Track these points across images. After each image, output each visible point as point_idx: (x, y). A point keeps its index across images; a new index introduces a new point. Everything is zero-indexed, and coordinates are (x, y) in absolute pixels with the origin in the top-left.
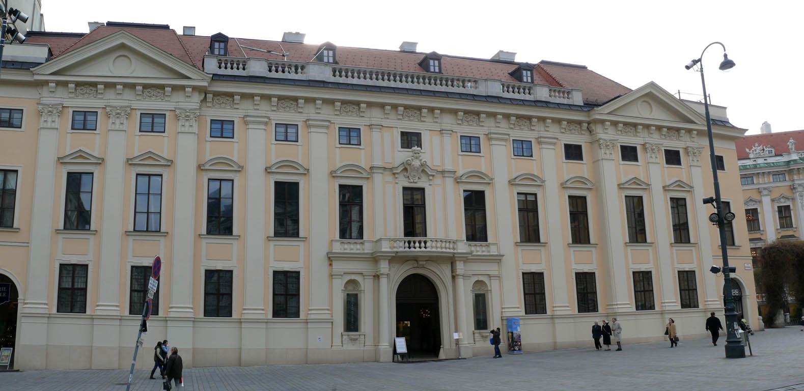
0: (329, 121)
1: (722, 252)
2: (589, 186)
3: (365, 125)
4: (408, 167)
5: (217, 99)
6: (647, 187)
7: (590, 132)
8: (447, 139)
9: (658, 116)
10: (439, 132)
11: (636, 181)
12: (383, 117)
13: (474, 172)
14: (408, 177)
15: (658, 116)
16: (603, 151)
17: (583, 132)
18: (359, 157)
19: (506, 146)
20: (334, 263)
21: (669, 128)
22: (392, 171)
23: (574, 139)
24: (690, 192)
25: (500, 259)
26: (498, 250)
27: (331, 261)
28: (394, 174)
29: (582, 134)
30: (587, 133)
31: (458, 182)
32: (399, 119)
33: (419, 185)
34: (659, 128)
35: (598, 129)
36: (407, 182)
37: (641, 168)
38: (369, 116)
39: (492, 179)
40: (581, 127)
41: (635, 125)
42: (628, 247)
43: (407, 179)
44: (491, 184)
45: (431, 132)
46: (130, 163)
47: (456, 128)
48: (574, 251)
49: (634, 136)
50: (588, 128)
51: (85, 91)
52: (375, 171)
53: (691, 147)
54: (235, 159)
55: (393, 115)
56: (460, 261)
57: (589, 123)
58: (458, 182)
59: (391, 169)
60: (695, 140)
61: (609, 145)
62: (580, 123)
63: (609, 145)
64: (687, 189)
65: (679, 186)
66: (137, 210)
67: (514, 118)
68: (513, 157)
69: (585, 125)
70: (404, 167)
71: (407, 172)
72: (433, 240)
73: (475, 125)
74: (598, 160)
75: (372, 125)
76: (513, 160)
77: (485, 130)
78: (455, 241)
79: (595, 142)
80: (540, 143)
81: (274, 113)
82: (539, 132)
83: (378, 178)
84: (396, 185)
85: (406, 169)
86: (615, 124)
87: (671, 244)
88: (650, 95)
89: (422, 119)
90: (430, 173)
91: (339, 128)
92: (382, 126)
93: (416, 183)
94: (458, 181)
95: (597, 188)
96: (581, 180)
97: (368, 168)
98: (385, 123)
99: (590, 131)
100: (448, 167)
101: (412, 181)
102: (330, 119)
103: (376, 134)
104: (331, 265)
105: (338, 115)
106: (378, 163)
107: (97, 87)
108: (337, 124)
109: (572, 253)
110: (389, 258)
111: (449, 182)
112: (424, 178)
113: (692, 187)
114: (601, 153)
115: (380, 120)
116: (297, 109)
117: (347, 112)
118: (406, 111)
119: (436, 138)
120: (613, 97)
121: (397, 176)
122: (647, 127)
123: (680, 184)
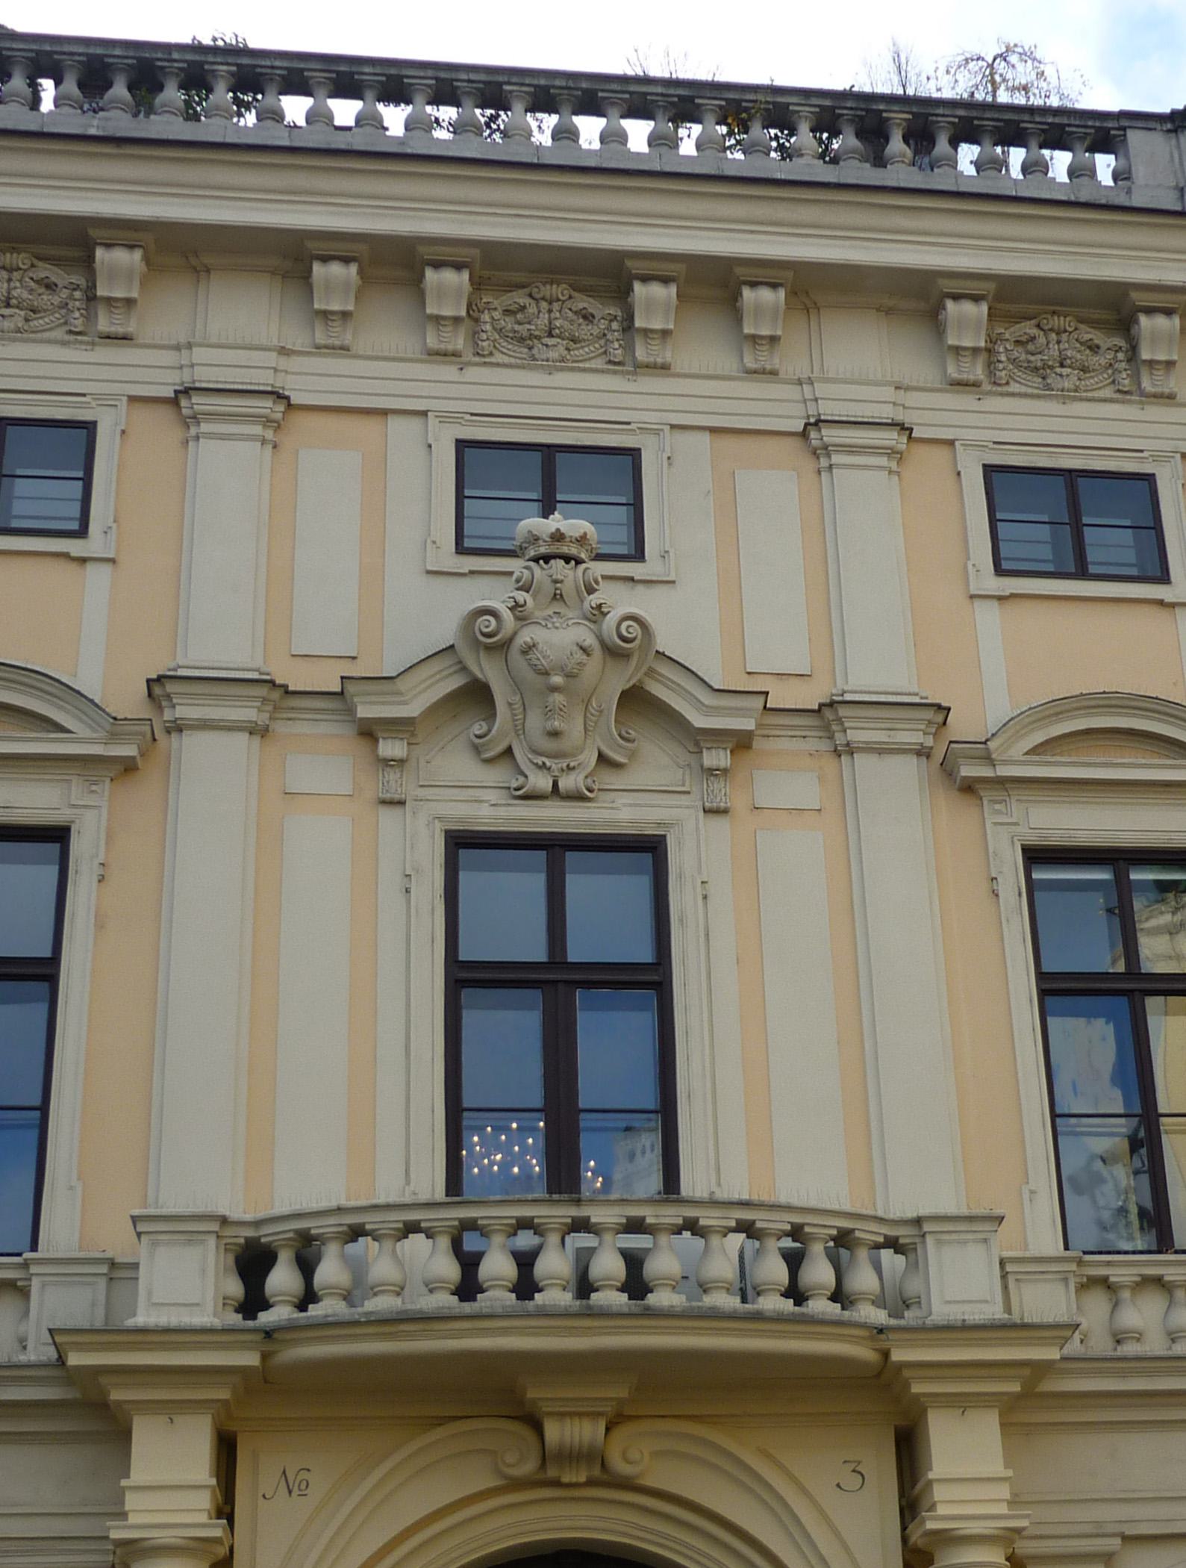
1: (1124, 1096)
4: (490, 671)
5: (507, 312)
8: (865, 493)
10: (166, 413)
12: (298, 339)
13: (1059, 708)
14: (509, 751)
22: (358, 716)
28: (369, 732)
31: (969, 788)
33: (618, 812)
43: (498, 775)
47: (938, 412)
49: (1123, 394)
51: (543, 320)
52: (184, 711)
55: (385, 331)
58: (969, 788)
70: (455, 683)
72: (762, 1219)
73: (1107, 392)
76: (988, 616)
78: (904, 1233)
82: (184, 357)
83: (213, 769)
85: (476, 695)
89: (641, 354)
91: (462, 445)
93: (578, 797)
94: (965, 776)
97: (126, 698)
98: (310, 379)
101: (541, 782)
102: (907, 418)
103: (228, 465)
106: (223, 643)
107: (87, 263)
108: (446, 418)
111: (894, 792)
112: (657, 762)
115: (272, 359)
116: (90, 317)
118: (1010, 333)
119: (774, 487)
121: (390, 748)
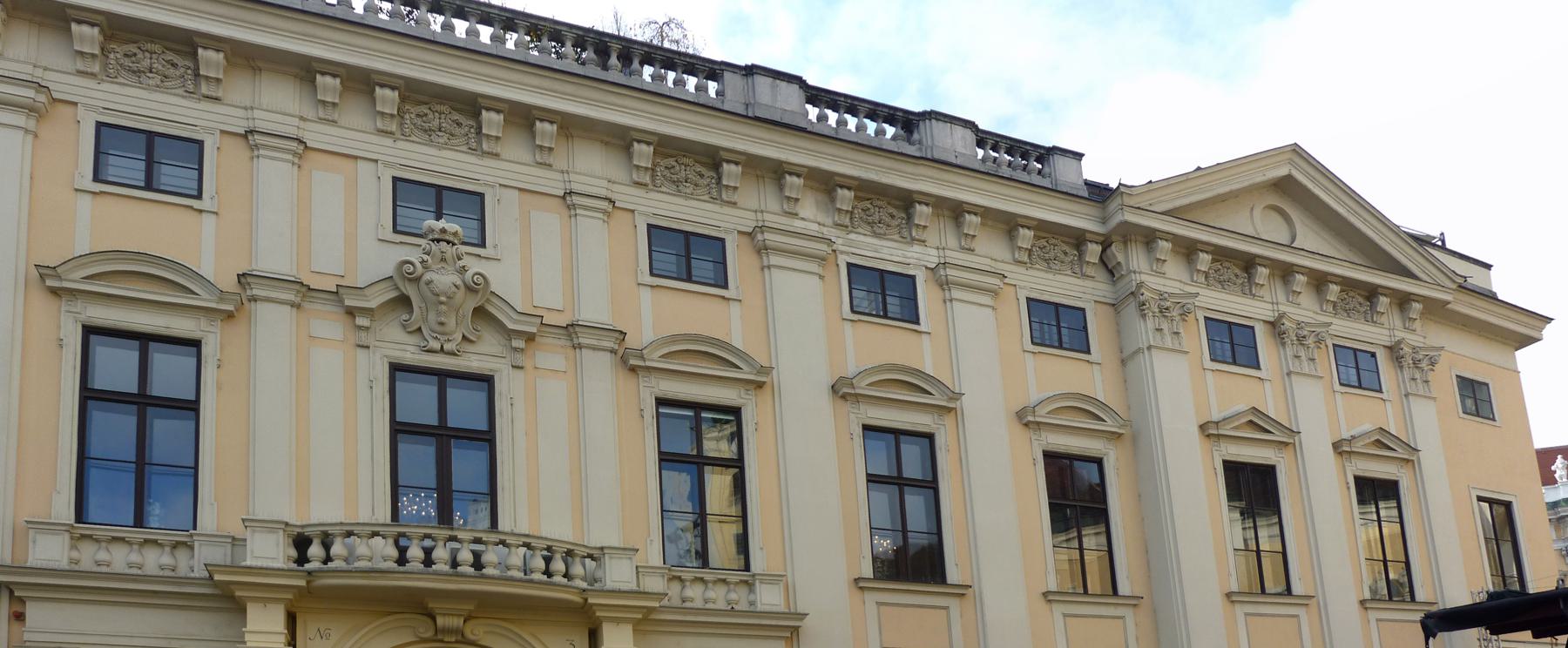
0: (40, 87)
2: (1110, 425)
3: (223, 132)
4: (410, 291)
6: (1288, 438)
7: (1111, 273)
8: (591, 228)
9: (1313, 246)
11: (1258, 422)
13: (675, 339)
14: (419, 329)
15: (1313, 246)
16: (1150, 323)
17: (1089, 271)
18: (197, 240)
19: (821, 277)
20: (33, 612)
21: (1348, 284)
23: (1061, 286)
24: (1290, 447)
25: (797, 629)
26: (788, 591)
27: (22, 601)
28: (351, 312)
29: (1084, 276)
30: (1101, 275)
32: (638, 184)
34: (1320, 281)
35: (1135, 260)
36: (412, 349)
37: (1267, 385)
38: (755, 207)
39: (766, 370)
40: (1081, 255)
41: (1248, 263)
42: (1238, 606)
43: (414, 339)
44: (767, 389)
45: (528, 197)
46: (842, 391)
47: (627, 195)
48: (879, 604)
50: (1101, 258)
53: (1291, 320)
54: (207, 271)
56: (618, 621)
57: (1106, 244)
59: (336, 294)
60: (1417, 325)
61: (1171, 310)
62: (1078, 239)
63: (1171, 310)
64: (1401, 453)
65: (1379, 443)
66: (95, 449)
67: (1030, 233)
68: (1337, 387)
69: (1093, 251)
70: (393, 294)
71: (411, 311)
74: (1139, 351)
75: (251, 132)
76: (848, 325)
77: (932, 258)
79: (1127, 300)
80: (944, 284)
81: (1021, 270)
83: (273, 322)
84: (361, 353)
86: (1188, 250)
87: (1362, 602)
88: (1286, 186)
90: (511, 326)
92: (301, 142)
94: (631, 364)
95: (1133, 434)
96: (1085, 408)
97: (228, 283)
98: (317, 135)
99: (1110, 269)
100: (594, 311)
103: (274, 172)
104: (19, 617)
105: (93, 75)
108: (387, 164)
109: (871, 608)
110: (290, 596)
111: (599, 367)
113: (957, 396)
114: (1143, 331)
117: (676, 183)
119: (549, 221)
120: (783, 85)
122: (1285, 272)
123: (1383, 442)
